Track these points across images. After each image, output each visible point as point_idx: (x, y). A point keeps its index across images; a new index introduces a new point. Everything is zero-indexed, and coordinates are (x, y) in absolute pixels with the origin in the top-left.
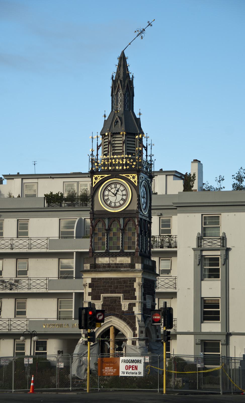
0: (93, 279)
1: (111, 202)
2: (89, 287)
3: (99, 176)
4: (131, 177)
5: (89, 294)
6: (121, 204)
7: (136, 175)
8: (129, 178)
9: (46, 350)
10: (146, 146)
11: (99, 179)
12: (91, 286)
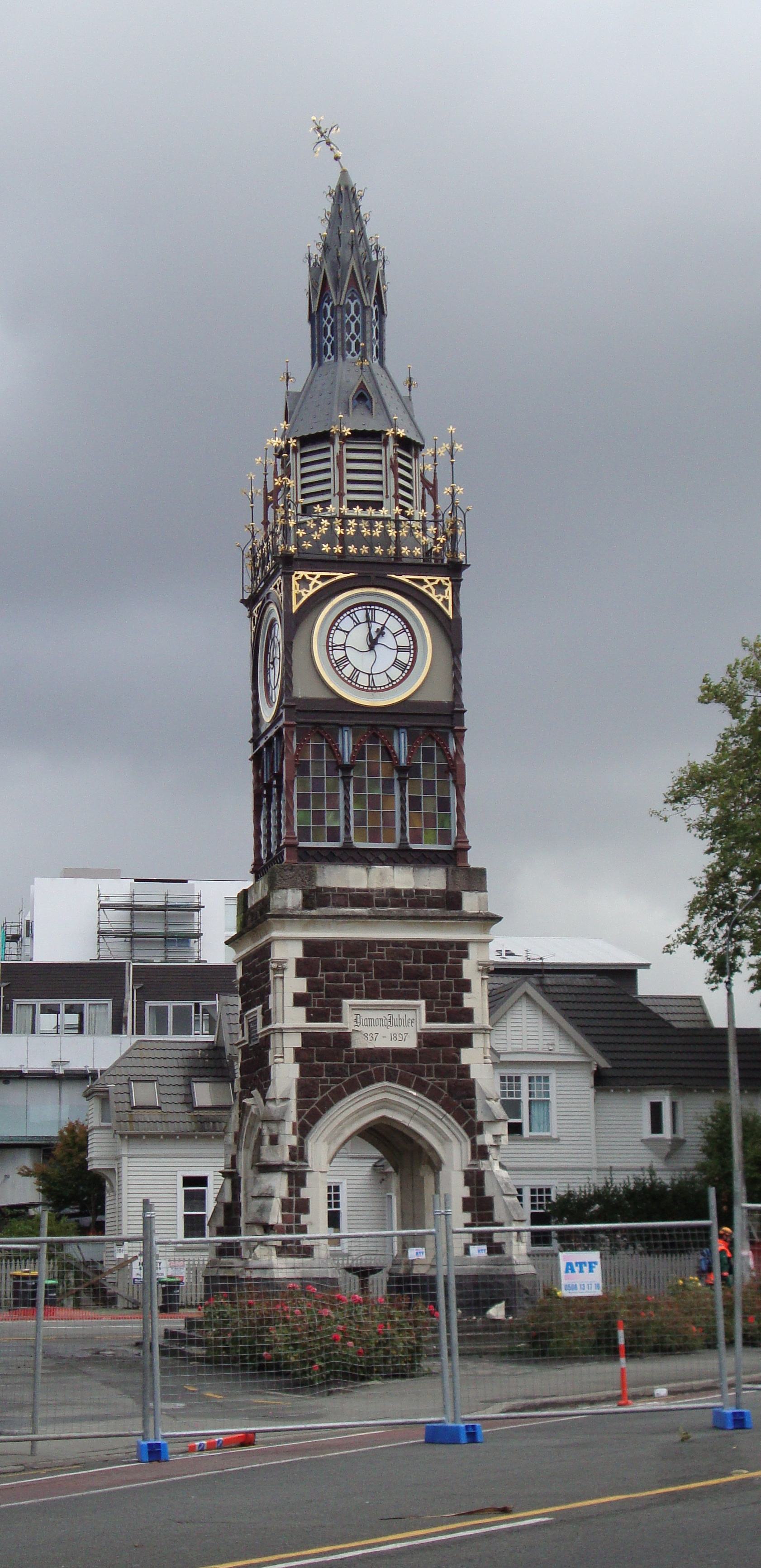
0: (310, 946)
1: (356, 669)
2: (299, 973)
3: (313, 576)
4: (430, 585)
5: (299, 1000)
6: (393, 681)
7: (447, 581)
8: (423, 589)
9: (204, 1210)
10: (432, 483)
11: (315, 585)
12: (302, 969)
